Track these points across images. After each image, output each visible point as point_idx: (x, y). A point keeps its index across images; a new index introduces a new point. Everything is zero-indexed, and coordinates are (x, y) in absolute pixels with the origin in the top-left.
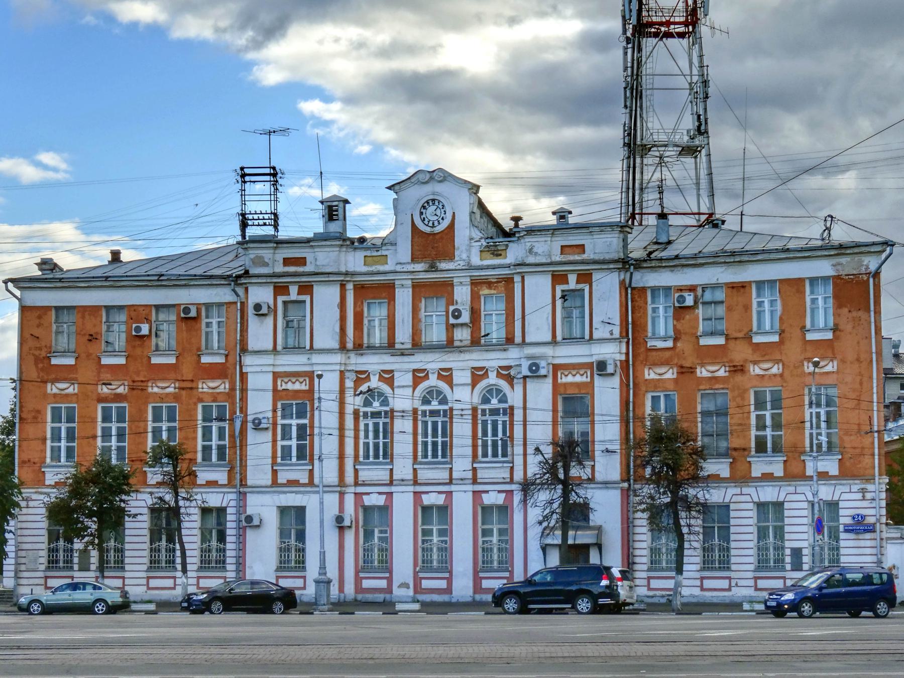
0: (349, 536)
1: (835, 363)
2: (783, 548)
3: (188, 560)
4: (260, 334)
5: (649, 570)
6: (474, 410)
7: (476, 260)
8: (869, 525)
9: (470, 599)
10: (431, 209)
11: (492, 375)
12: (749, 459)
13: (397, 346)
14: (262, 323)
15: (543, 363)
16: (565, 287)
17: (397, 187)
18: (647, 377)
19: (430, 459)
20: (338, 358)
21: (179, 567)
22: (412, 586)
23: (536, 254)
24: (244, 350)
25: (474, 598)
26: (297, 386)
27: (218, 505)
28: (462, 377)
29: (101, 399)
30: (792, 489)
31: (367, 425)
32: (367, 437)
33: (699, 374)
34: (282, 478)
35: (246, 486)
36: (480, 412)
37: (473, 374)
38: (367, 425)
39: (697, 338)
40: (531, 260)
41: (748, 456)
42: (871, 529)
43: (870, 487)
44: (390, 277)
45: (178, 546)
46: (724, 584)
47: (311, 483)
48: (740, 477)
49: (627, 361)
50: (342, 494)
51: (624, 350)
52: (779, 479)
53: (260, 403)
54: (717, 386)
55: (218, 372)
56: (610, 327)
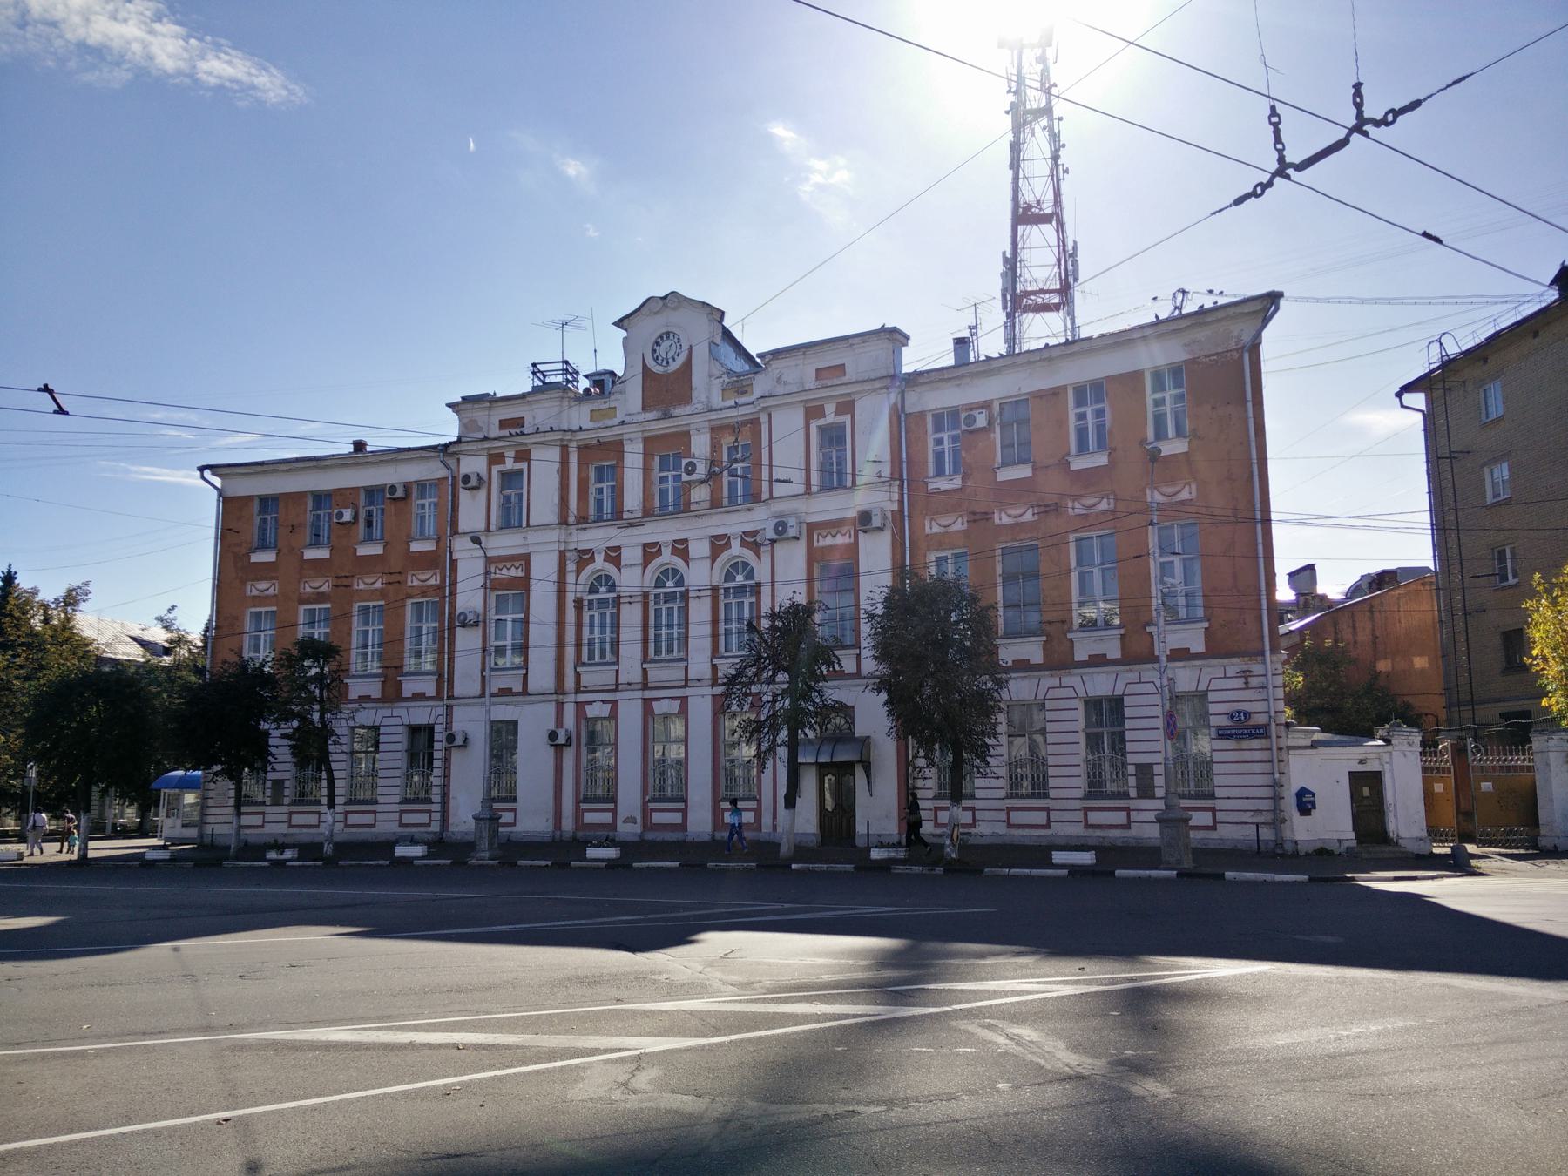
0: (569, 756)
1: (1194, 487)
2: (1125, 765)
3: (337, 792)
4: (472, 511)
5: (1088, 796)
6: (645, 595)
7: (717, 401)
8: (1257, 727)
9: (707, 838)
10: (665, 344)
11: (735, 544)
12: (1069, 636)
13: (625, 516)
14: (474, 498)
15: (792, 522)
16: (822, 422)
17: (626, 322)
18: (928, 531)
19: (664, 655)
20: (554, 535)
21: (324, 801)
22: (639, 820)
23: (785, 383)
24: (455, 532)
25: (713, 836)
26: (513, 573)
27: (425, 722)
28: (700, 549)
29: (302, 601)
30: (1133, 676)
31: (592, 617)
32: (592, 632)
33: (997, 521)
34: (497, 684)
35: (451, 697)
36: (652, 597)
37: (712, 544)
38: (592, 617)
39: (994, 471)
40: (780, 390)
41: (1071, 630)
42: (1261, 732)
43: (1257, 668)
44: (617, 431)
45: (324, 775)
46: (1040, 818)
47: (525, 692)
48: (1059, 661)
49: (901, 511)
50: (560, 706)
51: (896, 497)
52: (1114, 662)
53: (469, 598)
54: (1022, 536)
55: (430, 561)
56: (879, 467)
